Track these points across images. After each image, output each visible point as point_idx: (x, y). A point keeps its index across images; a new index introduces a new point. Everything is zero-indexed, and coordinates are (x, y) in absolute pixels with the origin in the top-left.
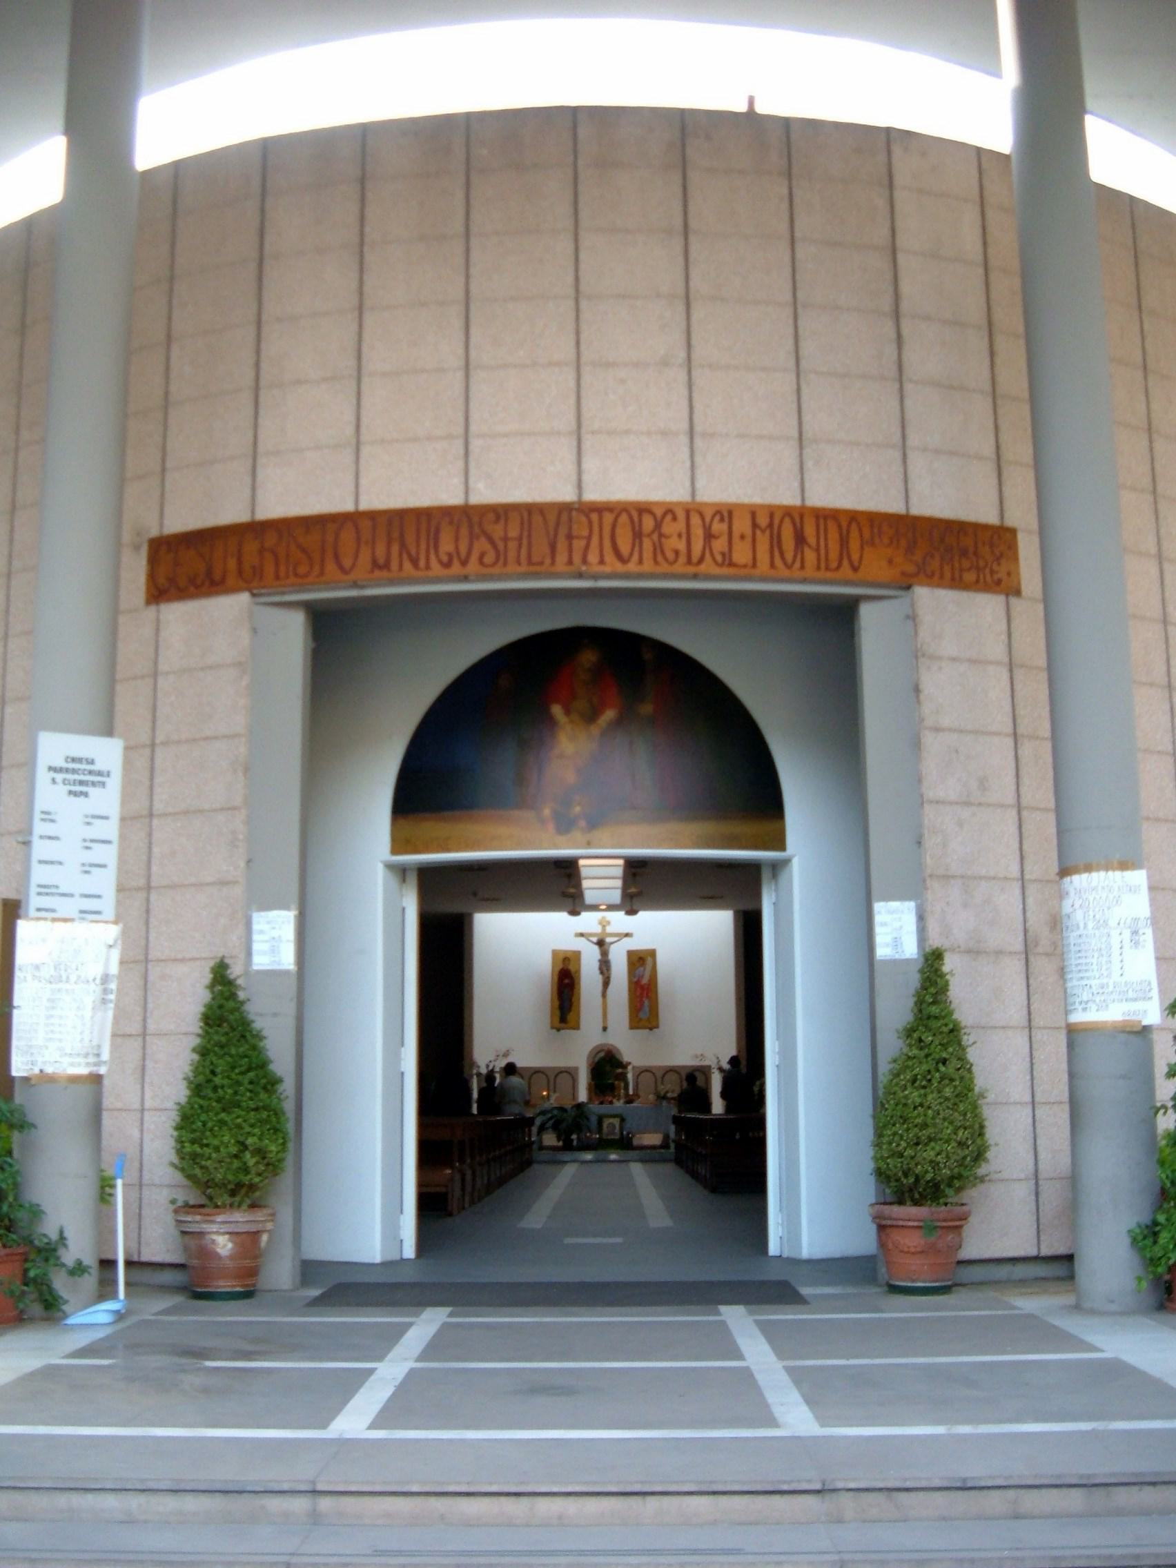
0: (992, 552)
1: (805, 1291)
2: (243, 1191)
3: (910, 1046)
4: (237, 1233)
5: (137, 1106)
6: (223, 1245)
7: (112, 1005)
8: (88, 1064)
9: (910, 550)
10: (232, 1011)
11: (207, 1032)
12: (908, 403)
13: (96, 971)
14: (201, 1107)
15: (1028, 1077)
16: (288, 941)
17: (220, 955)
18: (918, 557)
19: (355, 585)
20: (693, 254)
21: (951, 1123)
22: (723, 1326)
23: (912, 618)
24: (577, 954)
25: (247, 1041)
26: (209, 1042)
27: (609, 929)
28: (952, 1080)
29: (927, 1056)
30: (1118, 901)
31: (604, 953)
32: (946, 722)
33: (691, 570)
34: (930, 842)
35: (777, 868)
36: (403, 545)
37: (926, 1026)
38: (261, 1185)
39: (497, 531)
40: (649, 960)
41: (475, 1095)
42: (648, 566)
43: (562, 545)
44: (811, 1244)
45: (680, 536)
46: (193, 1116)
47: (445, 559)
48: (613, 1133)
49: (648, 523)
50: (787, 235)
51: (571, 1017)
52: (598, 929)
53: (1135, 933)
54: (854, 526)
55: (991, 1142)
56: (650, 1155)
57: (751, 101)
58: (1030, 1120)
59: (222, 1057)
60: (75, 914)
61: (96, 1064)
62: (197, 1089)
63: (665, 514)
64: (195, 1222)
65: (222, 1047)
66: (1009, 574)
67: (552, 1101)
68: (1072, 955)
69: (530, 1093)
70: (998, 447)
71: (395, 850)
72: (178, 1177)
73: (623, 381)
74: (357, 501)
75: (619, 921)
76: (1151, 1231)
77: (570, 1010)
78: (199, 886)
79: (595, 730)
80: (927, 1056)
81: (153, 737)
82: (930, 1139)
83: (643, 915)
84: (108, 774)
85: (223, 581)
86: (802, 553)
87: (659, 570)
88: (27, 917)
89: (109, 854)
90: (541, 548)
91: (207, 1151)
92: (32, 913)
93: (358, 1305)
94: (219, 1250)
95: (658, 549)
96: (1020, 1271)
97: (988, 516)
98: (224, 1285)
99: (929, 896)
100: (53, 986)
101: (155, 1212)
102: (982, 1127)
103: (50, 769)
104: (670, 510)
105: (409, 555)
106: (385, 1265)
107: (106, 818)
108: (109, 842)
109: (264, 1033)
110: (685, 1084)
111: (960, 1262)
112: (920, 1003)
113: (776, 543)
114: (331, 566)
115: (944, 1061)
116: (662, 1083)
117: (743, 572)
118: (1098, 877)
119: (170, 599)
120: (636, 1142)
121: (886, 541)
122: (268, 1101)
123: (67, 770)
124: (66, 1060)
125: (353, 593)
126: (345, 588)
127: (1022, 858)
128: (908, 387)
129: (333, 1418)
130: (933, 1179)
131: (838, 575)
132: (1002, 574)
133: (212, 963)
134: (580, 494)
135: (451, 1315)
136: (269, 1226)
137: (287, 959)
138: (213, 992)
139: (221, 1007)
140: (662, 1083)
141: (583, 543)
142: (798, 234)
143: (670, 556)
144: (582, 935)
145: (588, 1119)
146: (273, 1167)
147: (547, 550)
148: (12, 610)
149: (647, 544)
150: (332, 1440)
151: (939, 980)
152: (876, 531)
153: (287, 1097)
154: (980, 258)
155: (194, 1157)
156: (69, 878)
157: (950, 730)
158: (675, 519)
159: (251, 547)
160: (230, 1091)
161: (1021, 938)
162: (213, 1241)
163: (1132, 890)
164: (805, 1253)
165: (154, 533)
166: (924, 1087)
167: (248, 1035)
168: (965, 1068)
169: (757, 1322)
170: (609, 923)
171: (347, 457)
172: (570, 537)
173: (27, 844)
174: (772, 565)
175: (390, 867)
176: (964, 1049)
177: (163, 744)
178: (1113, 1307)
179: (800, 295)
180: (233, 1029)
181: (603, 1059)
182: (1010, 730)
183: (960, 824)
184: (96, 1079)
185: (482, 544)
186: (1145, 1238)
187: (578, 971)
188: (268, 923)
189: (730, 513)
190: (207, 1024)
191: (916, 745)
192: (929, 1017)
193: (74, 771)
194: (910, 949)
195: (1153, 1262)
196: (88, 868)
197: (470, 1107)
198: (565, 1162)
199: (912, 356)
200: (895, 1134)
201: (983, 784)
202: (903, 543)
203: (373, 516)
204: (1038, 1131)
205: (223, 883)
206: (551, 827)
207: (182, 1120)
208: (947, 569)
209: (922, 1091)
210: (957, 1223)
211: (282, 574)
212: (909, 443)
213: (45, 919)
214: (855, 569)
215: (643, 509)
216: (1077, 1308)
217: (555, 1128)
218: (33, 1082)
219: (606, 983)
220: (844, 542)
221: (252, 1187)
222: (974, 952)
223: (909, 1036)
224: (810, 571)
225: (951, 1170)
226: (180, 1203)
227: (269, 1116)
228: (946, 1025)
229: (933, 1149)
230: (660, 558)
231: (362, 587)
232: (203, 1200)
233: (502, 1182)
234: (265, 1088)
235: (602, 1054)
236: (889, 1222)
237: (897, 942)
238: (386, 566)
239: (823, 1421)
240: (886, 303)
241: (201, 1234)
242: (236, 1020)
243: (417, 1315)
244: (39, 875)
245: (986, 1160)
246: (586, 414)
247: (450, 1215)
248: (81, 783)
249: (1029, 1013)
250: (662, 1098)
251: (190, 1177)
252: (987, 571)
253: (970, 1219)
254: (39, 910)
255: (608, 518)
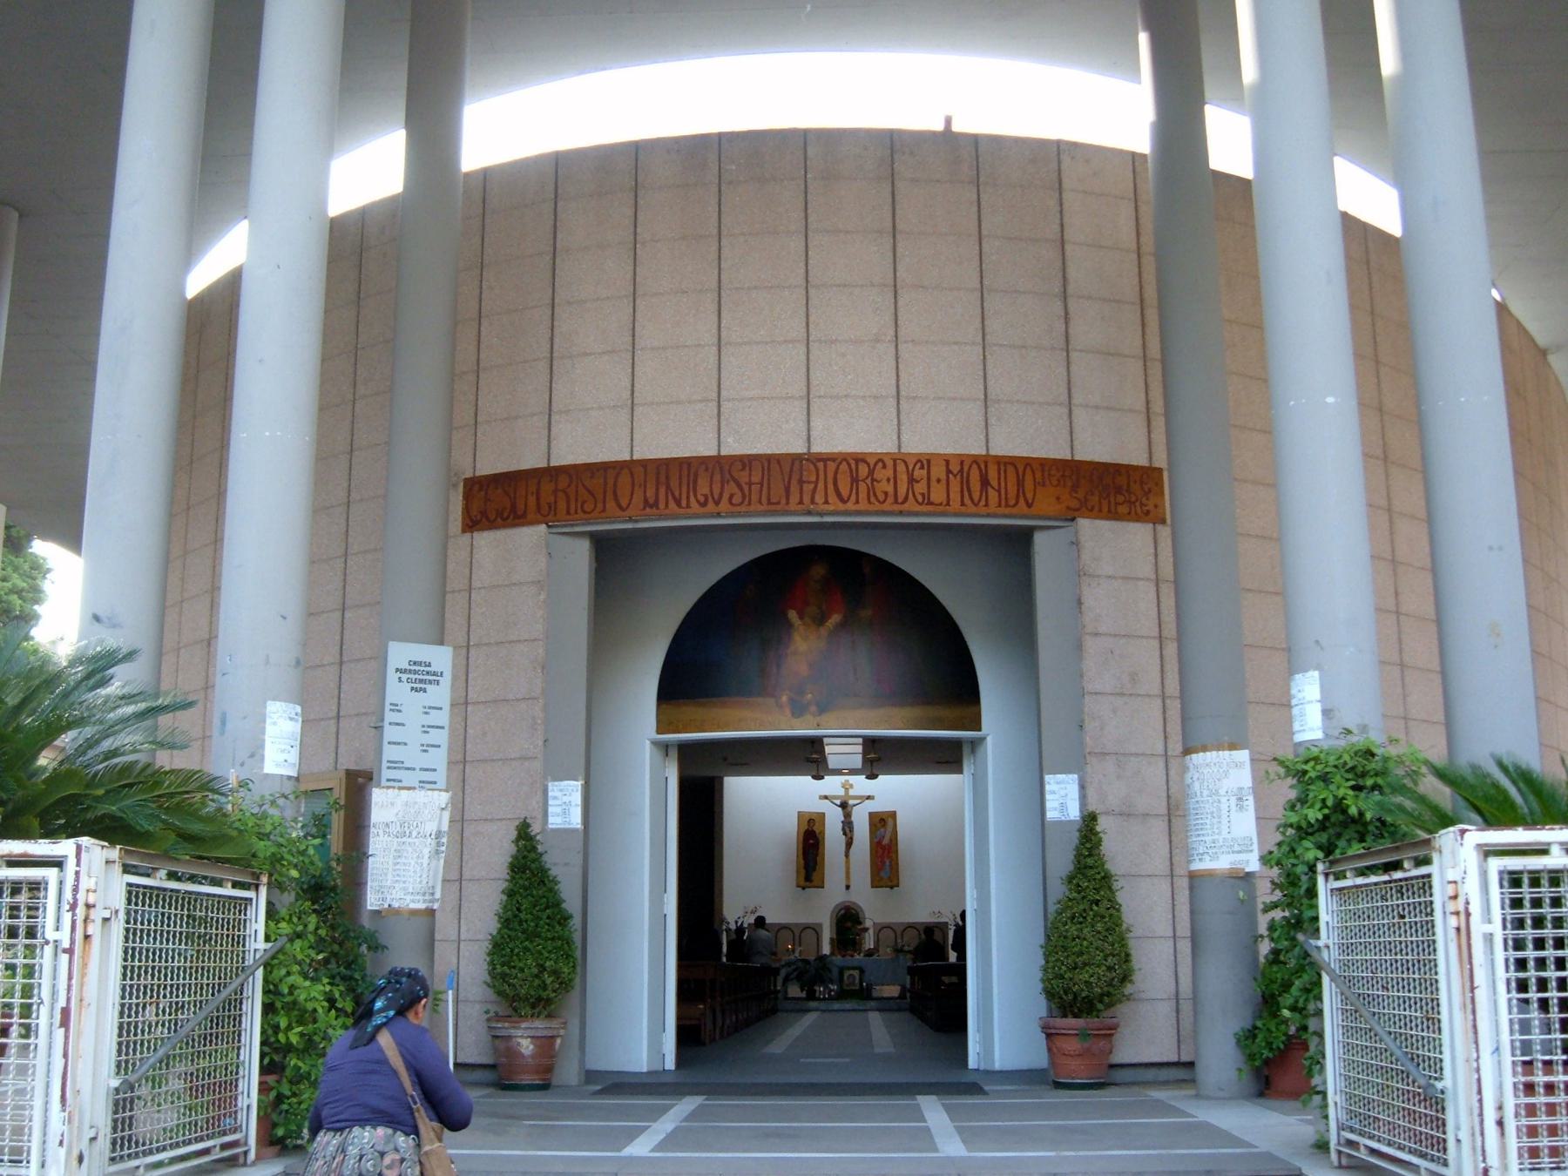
0: (1142, 489)
1: (986, 1088)
2: (543, 1003)
3: (1070, 890)
4: (538, 1037)
5: (454, 937)
6: (526, 1046)
7: (443, 855)
8: (424, 901)
9: (1075, 488)
10: (533, 861)
11: (513, 878)
12: (1073, 368)
13: (431, 827)
14: (509, 936)
15: (1170, 916)
16: (577, 805)
17: (523, 816)
18: (1081, 494)
19: (630, 520)
20: (900, 250)
21: (1102, 951)
22: (918, 1109)
23: (1076, 544)
24: (822, 815)
25: (545, 885)
26: (515, 885)
27: (852, 792)
28: (1103, 917)
29: (1084, 898)
30: (1226, 774)
31: (848, 815)
32: (1103, 629)
33: (896, 508)
34: (1090, 726)
35: (975, 744)
36: (668, 487)
37: (1083, 874)
38: (556, 999)
39: (743, 477)
40: (890, 822)
41: (725, 949)
42: (863, 506)
43: (794, 488)
44: (1001, 1059)
45: (888, 480)
46: (502, 944)
47: (702, 499)
48: (853, 984)
49: (863, 470)
50: (975, 231)
51: (815, 876)
52: (842, 792)
53: (1240, 799)
54: (1028, 471)
55: (1136, 967)
56: (886, 1006)
57: (948, 121)
58: (1172, 951)
59: (525, 897)
60: (417, 784)
61: (431, 901)
62: (506, 922)
63: (876, 464)
64: (504, 1028)
65: (526, 889)
66: (1156, 506)
67: (797, 954)
68: (1192, 817)
69: (776, 944)
70: (1148, 402)
71: (658, 732)
72: (490, 994)
73: (844, 355)
74: (632, 455)
75: (860, 784)
76: (1251, 1034)
77: (814, 870)
78: (505, 760)
79: (823, 631)
80: (1084, 898)
81: (468, 642)
82: (1085, 964)
83: (883, 779)
84: (441, 675)
85: (524, 515)
86: (987, 493)
87: (871, 508)
88: (379, 785)
89: (442, 737)
90: (778, 491)
91: (514, 972)
92: (384, 783)
93: (632, 1094)
94: (523, 1051)
95: (871, 492)
96: (1164, 1074)
97: (1140, 460)
98: (527, 1079)
99: (1089, 769)
100: (399, 840)
101: (469, 1023)
102: (1128, 955)
103: (397, 670)
104: (880, 460)
105: (673, 494)
106: (649, 1073)
107: (441, 709)
108: (442, 728)
109: (559, 879)
110: (923, 936)
111: (1112, 1066)
112: (1079, 856)
113: (965, 484)
114: (611, 504)
115: (1097, 903)
116: (902, 938)
117: (941, 508)
118: (1210, 756)
119: (482, 529)
120: (875, 994)
121: (1055, 483)
122: (561, 932)
123: (410, 671)
124: (409, 898)
125: (630, 526)
126: (623, 522)
127: (1166, 737)
128: (1074, 355)
129: (625, 1147)
130: (1087, 997)
131: (1014, 511)
132: (1151, 507)
133: (517, 823)
134: (809, 447)
135: (707, 1099)
136: (562, 1032)
137: (576, 820)
138: (518, 846)
139: (524, 857)
140: (902, 938)
141: (812, 486)
142: (984, 232)
143: (881, 497)
144: (826, 797)
145: (830, 971)
146: (565, 985)
147: (782, 492)
148: (350, 533)
149: (863, 487)
150: (625, 1157)
151: (1093, 838)
152: (1046, 473)
153: (576, 930)
154: (1134, 246)
155: (504, 976)
156: (411, 756)
157: (1105, 635)
158: (884, 467)
159: (547, 487)
160: (532, 924)
161: (1164, 803)
162: (519, 1044)
163: (1238, 765)
164: (997, 1066)
165: (469, 474)
166: (1081, 923)
167: (546, 880)
168: (1114, 906)
169: (943, 1105)
170: (851, 786)
171: (624, 416)
172: (801, 482)
173: (379, 728)
174: (963, 504)
175: (655, 743)
176: (1113, 893)
177: (477, 645)
178: (1221, 1094)
179: (986, 282)
180: (534, 876)
181: (844, 916)
182: (1156, 634)
183: (1114, 711)
184: (431, 912)
185: (731, 488)
186: (1246, 1040)
187: (823, 833)
188: (561, 790)
189: (929, 461)
190: (512, 871)
191: (1079, 647)
192: (1086, 867)
193: (415, 672)
194: (1074, 813)
195: (1251, 1057)
196: (425, 748)
197: (720, 958)
198: (808, 1010)
199: (1077, 328)
200: (1057, 960)
201: (1133, 678)
202: (1069, 484)
203: (644, 464)
204: (1179, 960)
205: (524, 758)
206: (788, 712)
207: (494, 947)
208: (1105, 503)
209: (1078, 926)
210: (1109, 1032)
211: (572, 511)
212: (1074, 401)
213: (394, 788)
214: (1029, 505)
215: (859, 459)
216: (1198, 1096)
217: (799, 978)
218: (383, 914)
219: (849, 844)
220: (1020, 484)
221: (548, 1001)
222: (1126, 814)
223: (1070, 882)
224: (993, 508)
225: (1101, 988)
226: (492, 1014)
227: (562, 945)
228: (1099, 873)
229: (1087, 971)
230: (872, 499)
231: (636, 521)
232: (510, 1012)
233: (748, 1023)
234: (559, 923)
235: (843, 912)
236: (1053, 1031)
237: (1063, 806)
238: (656, 505)
239: (969, 1151)
240: (1057, 288)
241: (510, 1037)
242: (537, 868)
243: (680, 1100)
244: (389, 753)
245: (1131, 981)
246: (814, 382)
247: (704, 1044)
248: (421, 681)
249: (1172, 864)
250: (898, 951)
251: (500, 993)
252: (1138, 504)
253: (1119, 1030)
254: (388, 780)
255: (832, 466)
